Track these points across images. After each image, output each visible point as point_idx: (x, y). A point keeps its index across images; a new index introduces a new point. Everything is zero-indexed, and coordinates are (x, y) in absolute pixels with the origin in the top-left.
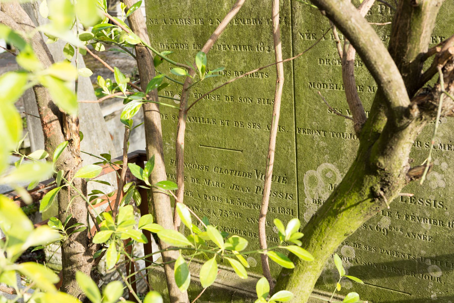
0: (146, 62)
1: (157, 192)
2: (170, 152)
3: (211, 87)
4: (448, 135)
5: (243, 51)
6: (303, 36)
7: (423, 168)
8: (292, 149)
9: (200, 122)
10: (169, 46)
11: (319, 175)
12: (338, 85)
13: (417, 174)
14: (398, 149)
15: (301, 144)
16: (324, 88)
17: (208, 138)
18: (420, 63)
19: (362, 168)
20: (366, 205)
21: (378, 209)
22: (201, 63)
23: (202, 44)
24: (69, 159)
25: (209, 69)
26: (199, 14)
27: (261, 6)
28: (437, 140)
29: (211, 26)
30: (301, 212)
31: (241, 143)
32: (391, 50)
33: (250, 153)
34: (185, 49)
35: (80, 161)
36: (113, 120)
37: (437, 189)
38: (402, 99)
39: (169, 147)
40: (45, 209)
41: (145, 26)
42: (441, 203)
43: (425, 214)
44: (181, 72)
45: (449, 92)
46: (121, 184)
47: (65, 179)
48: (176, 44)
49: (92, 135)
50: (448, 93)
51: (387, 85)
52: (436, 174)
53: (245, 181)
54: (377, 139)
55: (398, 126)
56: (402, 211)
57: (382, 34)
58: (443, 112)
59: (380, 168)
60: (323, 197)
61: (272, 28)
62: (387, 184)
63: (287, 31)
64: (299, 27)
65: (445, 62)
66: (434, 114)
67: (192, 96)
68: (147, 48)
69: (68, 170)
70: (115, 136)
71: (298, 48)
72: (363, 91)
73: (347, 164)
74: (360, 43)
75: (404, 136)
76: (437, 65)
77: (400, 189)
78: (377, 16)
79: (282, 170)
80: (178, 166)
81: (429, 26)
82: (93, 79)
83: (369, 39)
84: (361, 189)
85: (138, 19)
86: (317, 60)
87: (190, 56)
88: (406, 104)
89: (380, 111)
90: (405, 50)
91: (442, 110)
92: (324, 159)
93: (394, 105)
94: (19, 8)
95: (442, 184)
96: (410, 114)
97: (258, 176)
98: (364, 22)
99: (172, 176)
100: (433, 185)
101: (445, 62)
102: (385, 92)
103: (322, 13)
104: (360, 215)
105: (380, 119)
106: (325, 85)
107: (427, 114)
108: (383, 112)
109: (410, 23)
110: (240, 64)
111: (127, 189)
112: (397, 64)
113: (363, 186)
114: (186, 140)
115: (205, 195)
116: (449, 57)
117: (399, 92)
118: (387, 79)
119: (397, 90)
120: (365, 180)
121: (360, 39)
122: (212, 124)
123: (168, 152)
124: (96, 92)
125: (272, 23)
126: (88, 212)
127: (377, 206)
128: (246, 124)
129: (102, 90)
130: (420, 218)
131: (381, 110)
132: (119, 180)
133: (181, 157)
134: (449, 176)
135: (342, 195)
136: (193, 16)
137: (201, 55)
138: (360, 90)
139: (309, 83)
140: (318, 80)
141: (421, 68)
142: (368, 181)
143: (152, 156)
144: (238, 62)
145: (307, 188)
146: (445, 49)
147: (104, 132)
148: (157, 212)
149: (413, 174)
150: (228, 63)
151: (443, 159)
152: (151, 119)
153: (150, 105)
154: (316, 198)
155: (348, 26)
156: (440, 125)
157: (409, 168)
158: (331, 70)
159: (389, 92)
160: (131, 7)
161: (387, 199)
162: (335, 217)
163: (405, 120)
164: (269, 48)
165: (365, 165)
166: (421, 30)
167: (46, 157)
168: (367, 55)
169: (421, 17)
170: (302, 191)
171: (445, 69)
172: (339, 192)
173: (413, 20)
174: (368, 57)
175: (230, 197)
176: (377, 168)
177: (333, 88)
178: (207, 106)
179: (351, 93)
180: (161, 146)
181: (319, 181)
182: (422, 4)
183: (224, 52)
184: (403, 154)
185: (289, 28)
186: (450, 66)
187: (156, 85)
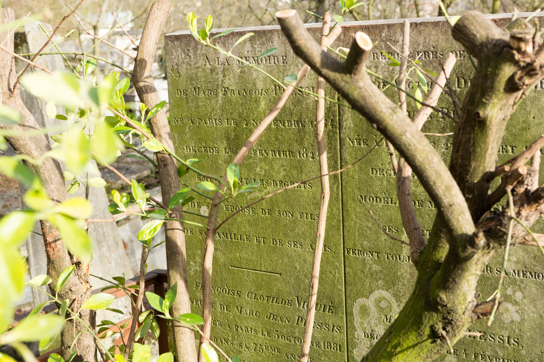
0: (169, 172)
1: (179, 326)
2: (196, 274)
3: (244, 198)
4: (522, 260)
5: (282, 157)
6: (352, 142)
7: (491, 304)
8: (339, 273)
9: (231, 238)
10: (197, 149)
11: (371, 304)
12: (394, 200)
13: (485, 311)
14: (463, 283)
15: (350, 267)
16: (376, 202)
17: (241, 258)
18: (486, 184)
19: (421, 303)
20: (426, 346)
21: (440, 351)
22: (233, 176)
23: (234, 149)
24: (76, 285)
25: (243, 177)
26: (232, 113)
27: (304, 106)
28: (509, 266)
29: (246, 128)
30: (350, 348)
31: (279, 264)
32: (452, 169)
33: (290, 276)
34: (215, 153)
35: (89, 287)
36: (127, 225)
37: (510, 323)
38: (465, 226)
39: (194, 268)
40: (46, 346)
41: (168, 129)
42: (516, 340)
43: (497, 352)
44: (210, 186)
45: (520, 217)
46: (136, 313)
47: (70, 310)
48: (204, 149)
49: (103, 246)
50: (518, 220)
51: (448, 209)
52: (509, 306)
53: (284, 309)
54: (438, 269)
55: (462, 256)
56: (470, 348)
57: (445, 141)
58: (513, 240)
59: (441, 304)
60: (376, 330)
61: (316, 134)
62: (450, 322)
63: (334, 136)
64: (348, 131)
65: (515, 183)
66: (503, 242)
67: (222, 208)
68: (170, 156)
69: (74, 298)
70: (129, 245)
71: (347, 156)
72: (422, 206)
73: (405, 292)
74: (417, 161)
75: (469, 267)
76: (506, 186)
77: (465, 328)
78: (438, 121)
79: (327, 298)
80: (205, 296)
81: (495, 142)
82: (109, 190)
83: (427, 157)
84: (419, 328)
85: (161, 122)
86: (369, 170)
87: (220, 162)
88: (470, 230)
89: (441, 237)
90: (468, 168)
91: (512, 237)
92: (378, 286)
93: (456, 232)
94: (22, 107)
95: (517, 318)
96: (475, 243)
97: (299, 304)
98: (421, 137)
99: (199, 306)
100: (506, 318)
101: (515, 183)
102: (446, 217)
103: (372, 126)
104: (419, 358)
105: (441, 247)
106: (378, 199)
107: (495, 242)
108: (445, 238)
109: (474, 138)
110: (278, 173)
111: (144, 318)
112: (459, 184)
113: (422, 324)
114: (215, 260)
115: (236, 325)
116: (519, 177)
117: (462, 218)
118: (448, 202)
119: (459, 215)
120: (424, 317)
121: (416, 156)
122: (246, 241)
123: (192, 273)
124: (110, 208)
125: (316, 126)
126: (97, 346)
127: (439, 348)
128: (285, 242)
129: (117, 206)
130: (491, 358)
131: (443, 236)
132: (133, 308)
133: (208, 284)
134: (525, 308)
135: (398, 334)
136: (225, 116)
137: (234, 167)
138: (419, 206)
139: (359, 197)
140: (370, 193)
141: (488, 189)
142: (427, 318)
143: (174, 283)
144: (276, 170)
145: (357, 320)
146: (515, 167)
147: (117, 243)
148: (179, 350)
149: (480, 311)
150: (265, 171)
151: (517, 287)
152: (174, 238)
153: (173, 223)
154: (368, 331)
155: (402, 141)
156: (511, 256)
157: (475, 304)
158: (382, 182)
159: (450, 217)
160: (152, 108)
161: (451, 340)
162: (389, 360)
163: (470, 250)
164: (313, 154)
165: (424, 300)
166: (486, 147)
167: (49, 283)
168: (425, 174)
169: (486, 132)
170: (352, 323)
171: (515, 191)
172: (395, 330)
173: (477, 135)
174: (425, 177)
175: (266, 329)
176: (438, 304)
177: (387, 203)
178: (240, 220)
179: (407, 215)
180: (185, 271)
181: (372, 311)
182: (487, 117)
183: (260, 159)
184: (469, 288)
185: (336, 132)
186: (520, 187)
187: (181, 201)
